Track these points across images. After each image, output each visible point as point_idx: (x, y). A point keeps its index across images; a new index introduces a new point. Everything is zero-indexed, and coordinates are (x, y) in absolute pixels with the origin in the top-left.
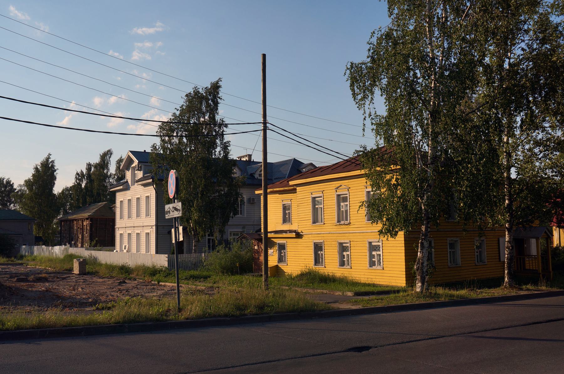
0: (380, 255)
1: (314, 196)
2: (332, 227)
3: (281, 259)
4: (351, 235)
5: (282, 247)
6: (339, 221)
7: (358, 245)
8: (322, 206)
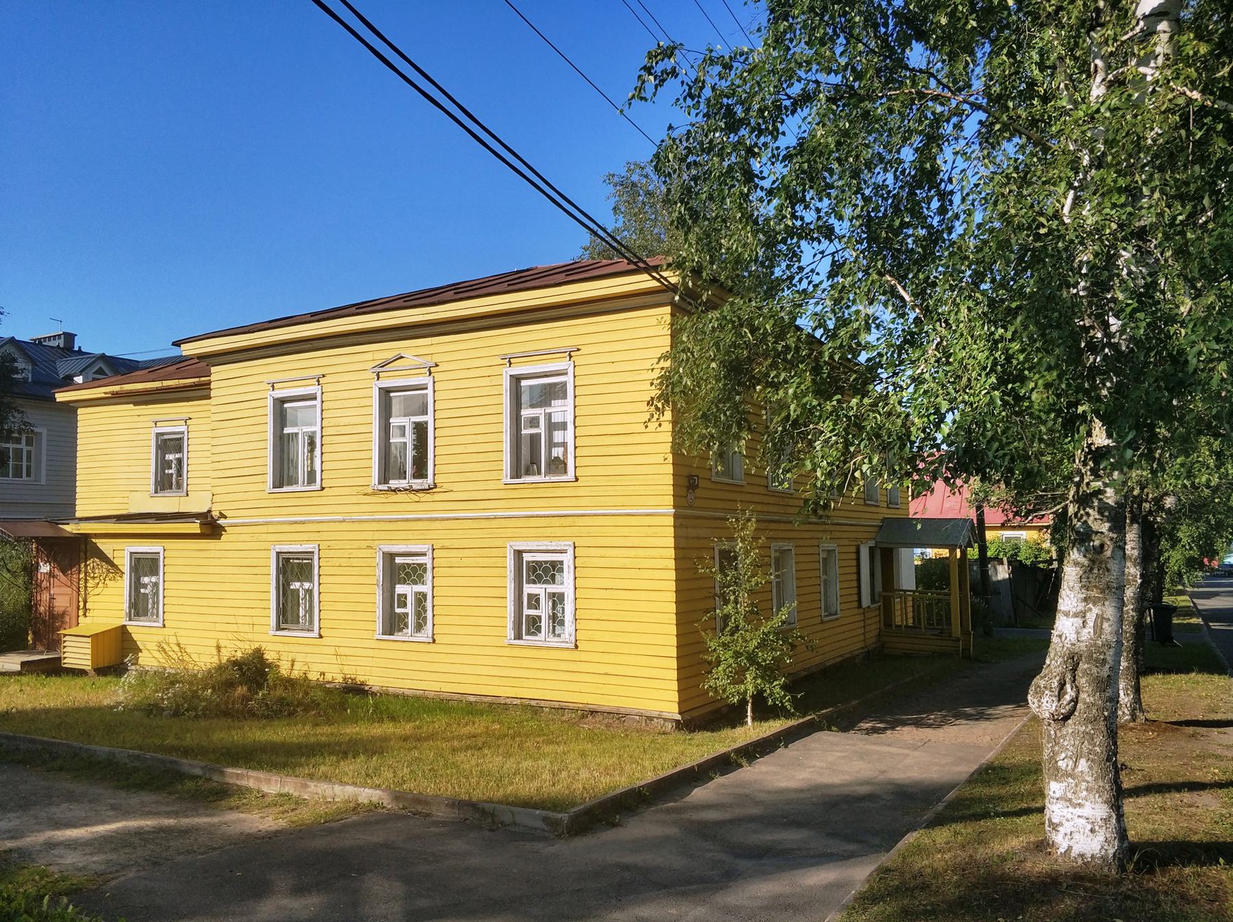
0: (425, 596)
1: (279, 394)
2: (354, 500)
3: (139, 606)
4: (437, 525)
5: (145, 566)
6: (384, 479)
7: (465, 562)
8: (317, 429)
